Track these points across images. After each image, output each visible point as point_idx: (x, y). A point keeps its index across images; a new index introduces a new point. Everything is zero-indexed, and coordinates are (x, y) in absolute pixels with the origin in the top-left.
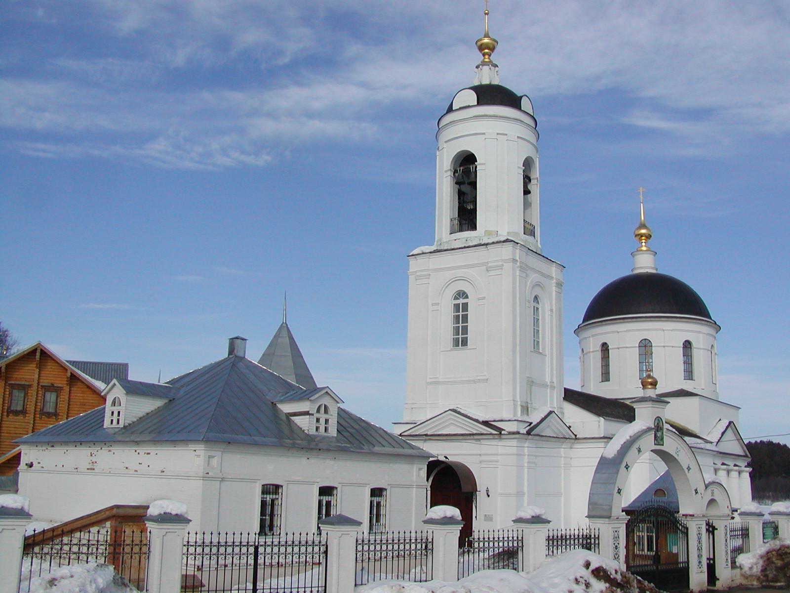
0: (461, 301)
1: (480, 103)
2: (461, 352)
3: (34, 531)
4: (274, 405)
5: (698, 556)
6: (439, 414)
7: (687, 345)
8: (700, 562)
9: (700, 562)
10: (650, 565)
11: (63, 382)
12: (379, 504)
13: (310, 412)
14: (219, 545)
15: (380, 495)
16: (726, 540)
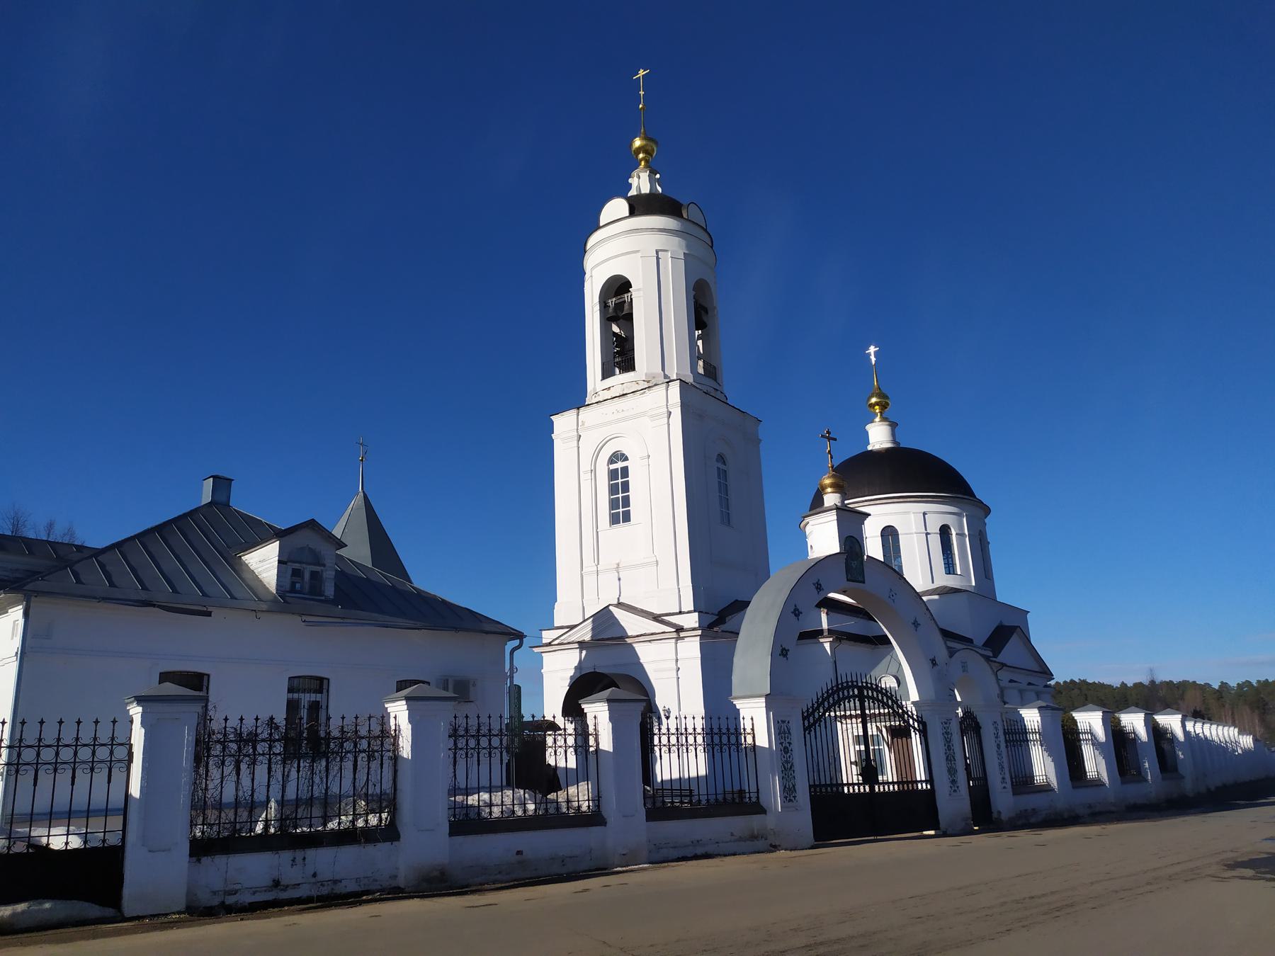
0: (619, 465)
1: (633, 212)
2: (622, 528)
4: (1047, 686)
5: (949, 771)
6: (632, 704)
7: (944, 531)
8: (953, 782)
9: (953, 782)
10: (858, 784)
16: (998, 746)
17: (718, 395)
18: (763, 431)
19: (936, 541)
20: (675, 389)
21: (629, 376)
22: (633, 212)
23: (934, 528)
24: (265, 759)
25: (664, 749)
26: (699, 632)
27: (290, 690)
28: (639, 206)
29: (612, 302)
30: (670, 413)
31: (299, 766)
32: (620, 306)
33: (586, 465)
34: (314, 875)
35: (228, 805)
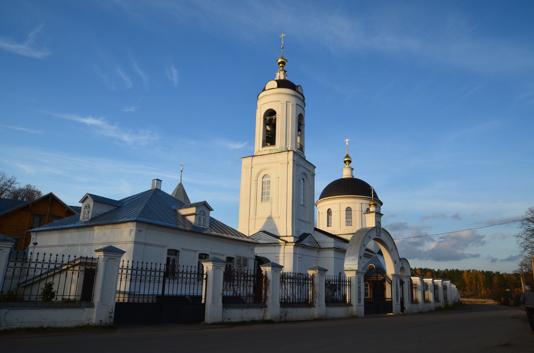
1: (279, 86)
3: (75, 257)
4: (176, 211)
7: (349, 210)
11: (304, 296)
12: (230, 266)
13: (299, 88)
14: (151, 270)
15: (231, 262)
17: (302, 155)
18: (316, 171)
19: (344, 214)
20: (291, 154)
21: (271, 148)
22: (279, 86)
23: (344, 209)
24: (77, 273)
25: (123, 276)
26: (294, 244)
27: (168, 254)
28: (282, 84)
29: (268, 118)
30: (288, 163)
31: (230, 284)
32: (271, 120)
33: (254, 178)
34: (17, 319)
35: (151, 295)
